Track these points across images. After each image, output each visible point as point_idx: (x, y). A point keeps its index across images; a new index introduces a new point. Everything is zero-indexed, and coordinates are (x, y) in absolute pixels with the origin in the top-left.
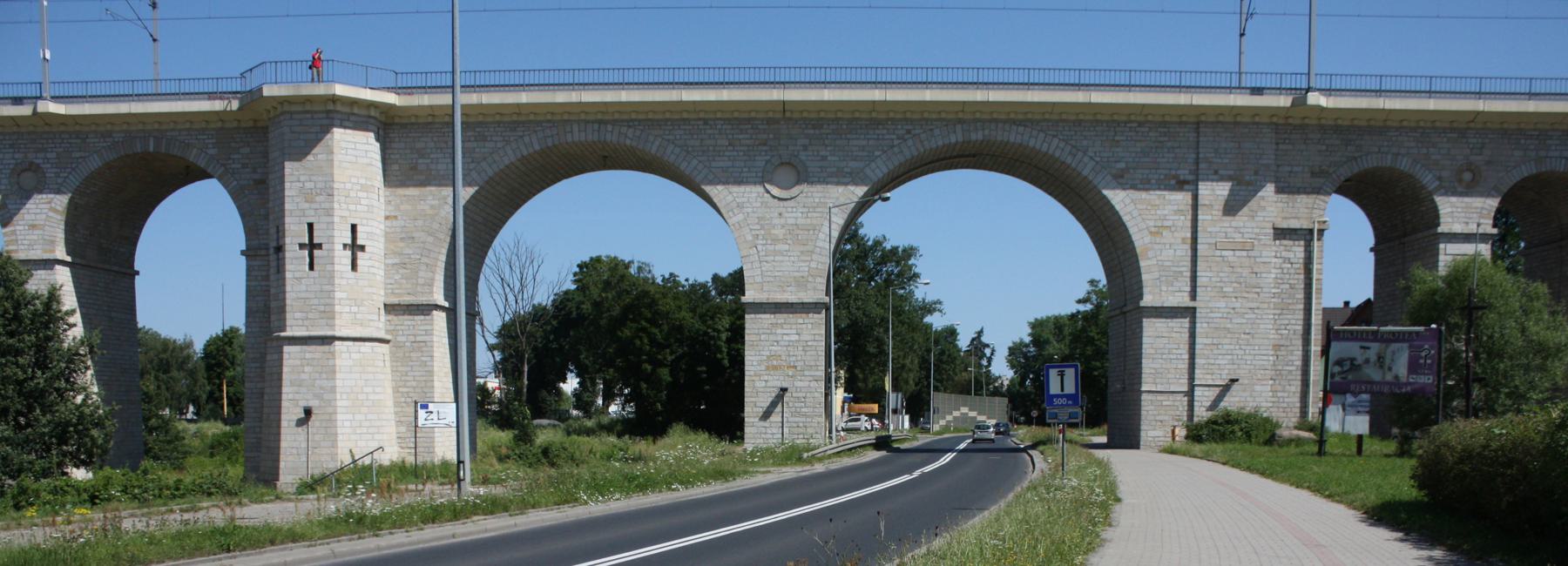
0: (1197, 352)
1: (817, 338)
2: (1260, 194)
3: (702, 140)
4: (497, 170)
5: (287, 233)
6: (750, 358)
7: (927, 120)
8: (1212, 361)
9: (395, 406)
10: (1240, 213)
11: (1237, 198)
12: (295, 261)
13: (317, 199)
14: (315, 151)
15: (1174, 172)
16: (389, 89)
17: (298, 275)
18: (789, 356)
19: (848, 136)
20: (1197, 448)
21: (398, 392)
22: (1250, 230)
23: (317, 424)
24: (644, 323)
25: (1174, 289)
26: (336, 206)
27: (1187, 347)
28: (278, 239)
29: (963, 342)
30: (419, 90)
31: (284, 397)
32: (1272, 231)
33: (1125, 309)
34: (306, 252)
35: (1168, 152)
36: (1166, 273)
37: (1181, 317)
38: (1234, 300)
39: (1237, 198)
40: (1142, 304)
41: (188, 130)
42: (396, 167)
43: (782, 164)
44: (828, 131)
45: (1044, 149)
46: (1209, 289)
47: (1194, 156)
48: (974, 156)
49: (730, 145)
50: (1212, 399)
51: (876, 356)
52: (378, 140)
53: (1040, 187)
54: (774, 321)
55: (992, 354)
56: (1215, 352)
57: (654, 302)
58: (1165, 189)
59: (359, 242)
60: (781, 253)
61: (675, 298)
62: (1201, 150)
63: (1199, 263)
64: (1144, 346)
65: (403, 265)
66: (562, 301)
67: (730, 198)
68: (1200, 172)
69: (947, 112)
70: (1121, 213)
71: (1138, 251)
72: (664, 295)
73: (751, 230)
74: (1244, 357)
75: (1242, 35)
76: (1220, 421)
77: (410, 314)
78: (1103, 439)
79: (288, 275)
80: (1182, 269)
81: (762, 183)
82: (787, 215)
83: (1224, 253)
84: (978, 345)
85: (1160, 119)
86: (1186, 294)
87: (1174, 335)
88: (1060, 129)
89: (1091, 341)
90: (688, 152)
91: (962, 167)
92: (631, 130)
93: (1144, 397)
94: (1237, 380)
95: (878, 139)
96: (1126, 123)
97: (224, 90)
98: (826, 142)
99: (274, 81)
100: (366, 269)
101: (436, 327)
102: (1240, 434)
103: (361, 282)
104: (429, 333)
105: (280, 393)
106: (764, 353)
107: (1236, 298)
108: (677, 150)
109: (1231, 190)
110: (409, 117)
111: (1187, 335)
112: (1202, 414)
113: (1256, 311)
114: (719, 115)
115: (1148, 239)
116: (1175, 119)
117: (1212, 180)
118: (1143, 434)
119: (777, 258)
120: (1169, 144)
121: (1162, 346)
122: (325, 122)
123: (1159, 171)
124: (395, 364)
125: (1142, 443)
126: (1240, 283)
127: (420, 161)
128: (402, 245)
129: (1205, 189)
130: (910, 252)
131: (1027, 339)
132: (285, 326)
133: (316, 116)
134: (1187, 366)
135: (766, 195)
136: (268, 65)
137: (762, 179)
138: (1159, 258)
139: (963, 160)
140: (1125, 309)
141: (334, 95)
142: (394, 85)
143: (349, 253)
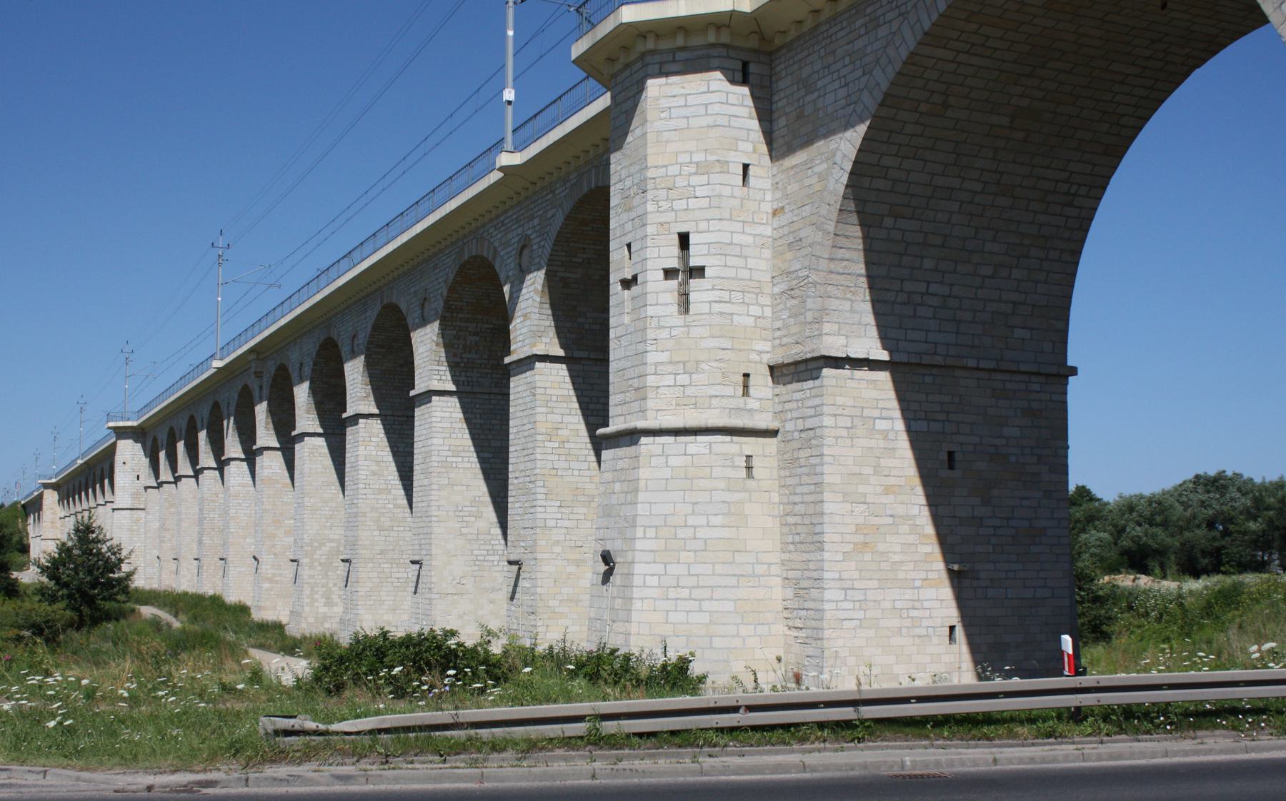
26: (650, 207)
77: (798, 381)
100: (706, 308)
124: (783, 473)
128: (789, 256)
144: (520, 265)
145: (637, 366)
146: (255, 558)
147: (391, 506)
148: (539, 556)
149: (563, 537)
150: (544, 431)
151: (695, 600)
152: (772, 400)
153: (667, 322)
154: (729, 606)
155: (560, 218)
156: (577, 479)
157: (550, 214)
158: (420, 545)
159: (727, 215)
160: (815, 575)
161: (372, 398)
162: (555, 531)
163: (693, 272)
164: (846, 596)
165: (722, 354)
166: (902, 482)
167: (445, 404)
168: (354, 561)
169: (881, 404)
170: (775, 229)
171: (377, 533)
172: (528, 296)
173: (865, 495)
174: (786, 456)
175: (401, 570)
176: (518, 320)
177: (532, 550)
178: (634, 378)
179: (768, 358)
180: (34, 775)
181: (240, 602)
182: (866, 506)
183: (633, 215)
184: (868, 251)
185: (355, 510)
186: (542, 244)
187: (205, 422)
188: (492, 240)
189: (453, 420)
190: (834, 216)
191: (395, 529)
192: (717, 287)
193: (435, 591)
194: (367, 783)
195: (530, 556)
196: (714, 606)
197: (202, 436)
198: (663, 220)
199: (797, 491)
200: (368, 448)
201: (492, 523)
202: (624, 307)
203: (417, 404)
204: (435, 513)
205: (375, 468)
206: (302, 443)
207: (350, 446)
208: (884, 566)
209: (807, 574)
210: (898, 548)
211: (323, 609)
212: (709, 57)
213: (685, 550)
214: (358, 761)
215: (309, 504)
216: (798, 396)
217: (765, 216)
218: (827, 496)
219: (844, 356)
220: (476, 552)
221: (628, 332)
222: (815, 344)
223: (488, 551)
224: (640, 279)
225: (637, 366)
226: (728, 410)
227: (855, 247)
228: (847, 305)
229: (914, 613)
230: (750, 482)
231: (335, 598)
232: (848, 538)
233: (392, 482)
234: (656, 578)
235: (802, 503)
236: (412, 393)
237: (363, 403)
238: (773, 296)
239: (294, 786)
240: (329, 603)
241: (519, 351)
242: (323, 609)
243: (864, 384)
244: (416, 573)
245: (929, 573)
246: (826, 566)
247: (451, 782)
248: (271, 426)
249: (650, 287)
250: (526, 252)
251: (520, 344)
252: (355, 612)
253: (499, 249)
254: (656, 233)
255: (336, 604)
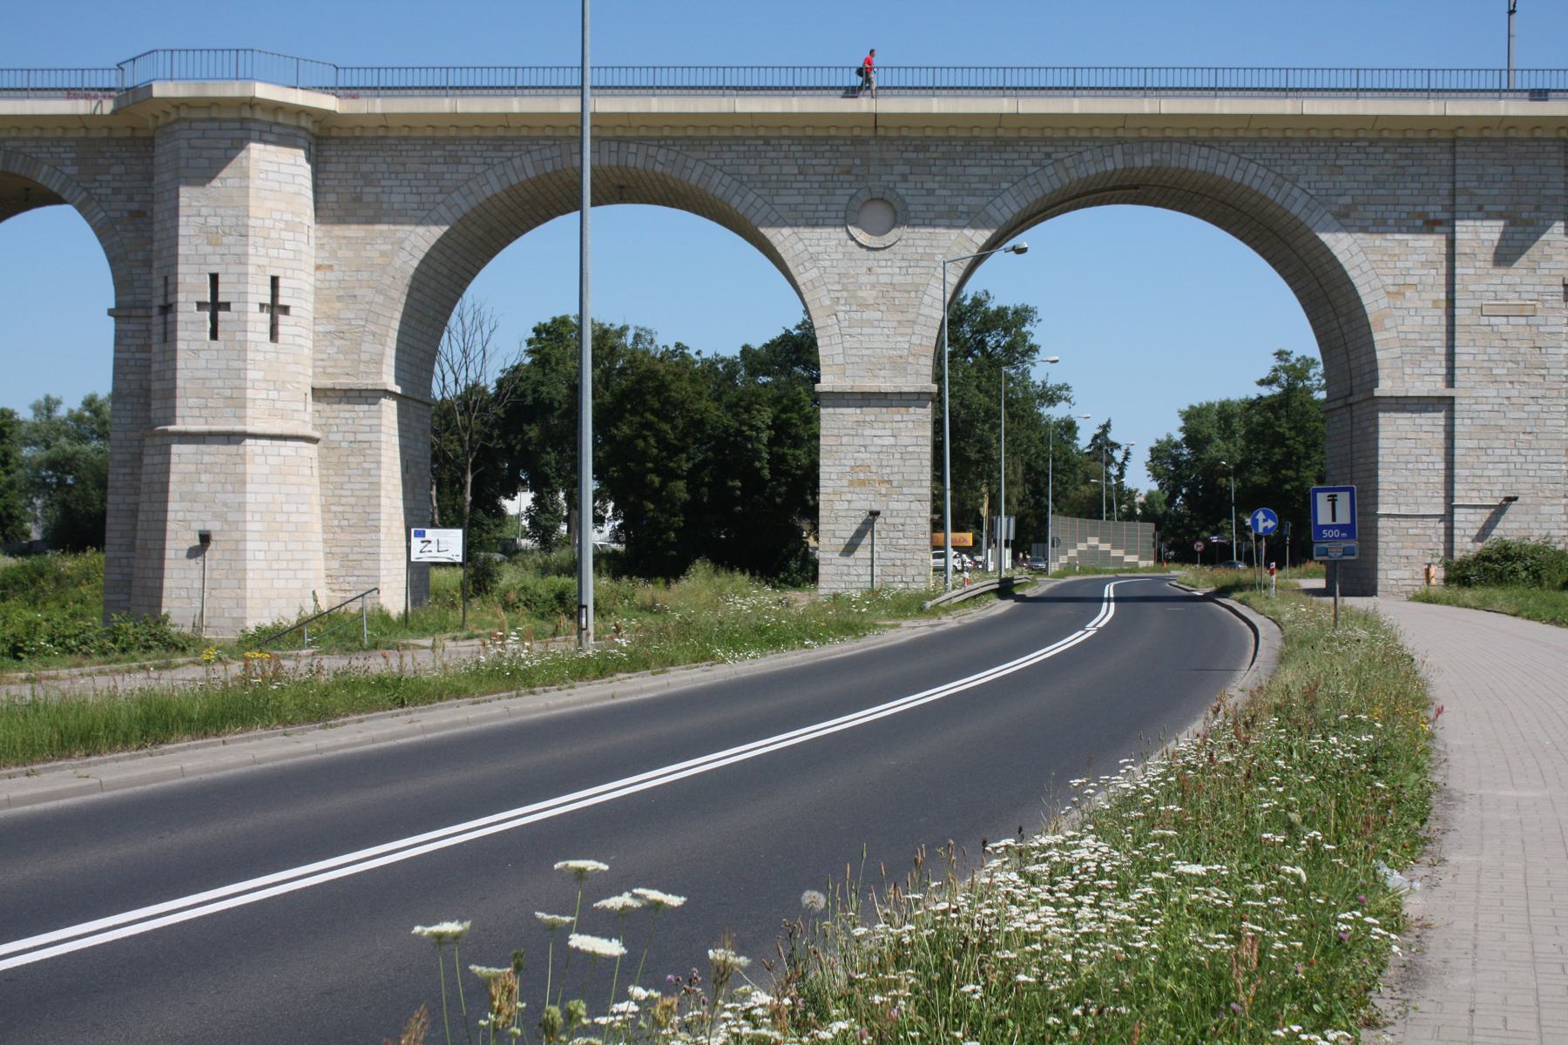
0: (1457, 459)
1: (921, 442)
2: (1544, 237)
3: (761, 166)
4: (474, 204)
5: (180, 288)
6: (827, 469)
7: (1073, 139)
8: (1479, 472)
9: (325, 532)
10: (1516, 265)
11: (1511, 243)
12: (190, 323)
13: (225, 240)
14: (223, 174)
15: (1419, 209)
16: (324, 89)
17: (194, 346)
18: (881, 466)
19: (966, 162)
20: (1468, 594)
21: (329, 511)
22: (1530, 288)
23: (218, 555)
24: (648, 415)
25: (1422, 371)
26: (251, 250)
27: (1442, 452)
28: (166, 295)
29: (1084, 440)
30: (369, 92)
31: (170, 516)
32: (1562, 289)
33: (1351, 400)
34: (207, 314)
35: (1412, 181)
36: (1412, 350)
37: (1434, 411)
38: (1508, 385)
39: (1511, 243)
40: (1377, 393)
41: (37, 139)
42: (332, 197)
43: (872, 199)
44: (935, 155)
45: (1237, 178)
46: (1472, 371)
47: (1449, 186)
48: (1136, 187)
49: (800, 173)
50: (1480, 525)
51: (977, 463)
52: (308, 160)
53: (1228, 228)
54: (861, 418)
55: (1126, 458)
56: (1484, 459)
57: (662, 388)
58: (1408, 232)
59: (282, 301)
60: (870, 323)
61: (693, 381)
62: (1458, 177)
63: (1457, 335)
64: (1381, 452)
65: (340, 334)
66: (512, 378)
67: (800, 246)
68: (1458, 208)
69: (1101, 129)
70: (1346, 267)
71: (1371, 319)
72: (678, 376)
73: (829, 291)
74: (1525, 466)
75: (1511, 12)
76: (1494, 557)
77: (348, 403)
78: (1320, 583)
79: (181, 345)
80: (1434, 343)
81: (844, 223)
82: (879, 271)
83: (1493, 320)
84: (1103, 445)
85: (1399, 136)
86: (1440, 379)
87: (1423, 435)
88: (1260, 150)
89: (1280, 440)
90: (742, 183)
91: (1117, 202)
92: (663, 151)
93: (1382, 523)
94: (1516, 499)
95: (1006, 166)
96: (1351, 141)
97: (93, 85)
98: (934, 169)
99: (168, 76)
100: (290, 340)
101: (384, 422)
102: (1524, 574)
103: (282, 357)
104: (375, 429)
105: (166, 511)
106: (846, 462)
107: (1511, 382)
108: (726, 181)
109: (1503, 233)
110: (352, 129)
111: (1442, 436)
112: (1466, 546)
113: (1541, 401)
114: (785, 132)
115: (1383, 303)
116: (1421, 135)
117: (1475, 219)
118: (1381, 575)
119: (866, 330)
120: (1412, 170)
121: (1406, 451)
122: (238, 134)
123: (1398, 208)
124: (325, 472)
125: (1379, 588)
126: (1517, 363)
127: (367, 190)
128: (338, 305)
129: (1465, 231)
130: (1023, 315)
131: (1179, 436)
132: (174, 416)
133: (225, 125)
134: (1442, 479)
135: (850, 242)
136: (161, 53)
137: (845, 220)
138: (1400, 328)
139: (1118, 192)
140: (1351, 400)
141: (253, 98)
142: (333, 84)
143: (267, 316)
198: (260, 263)
212: (296, 136)
241: (489, 382)
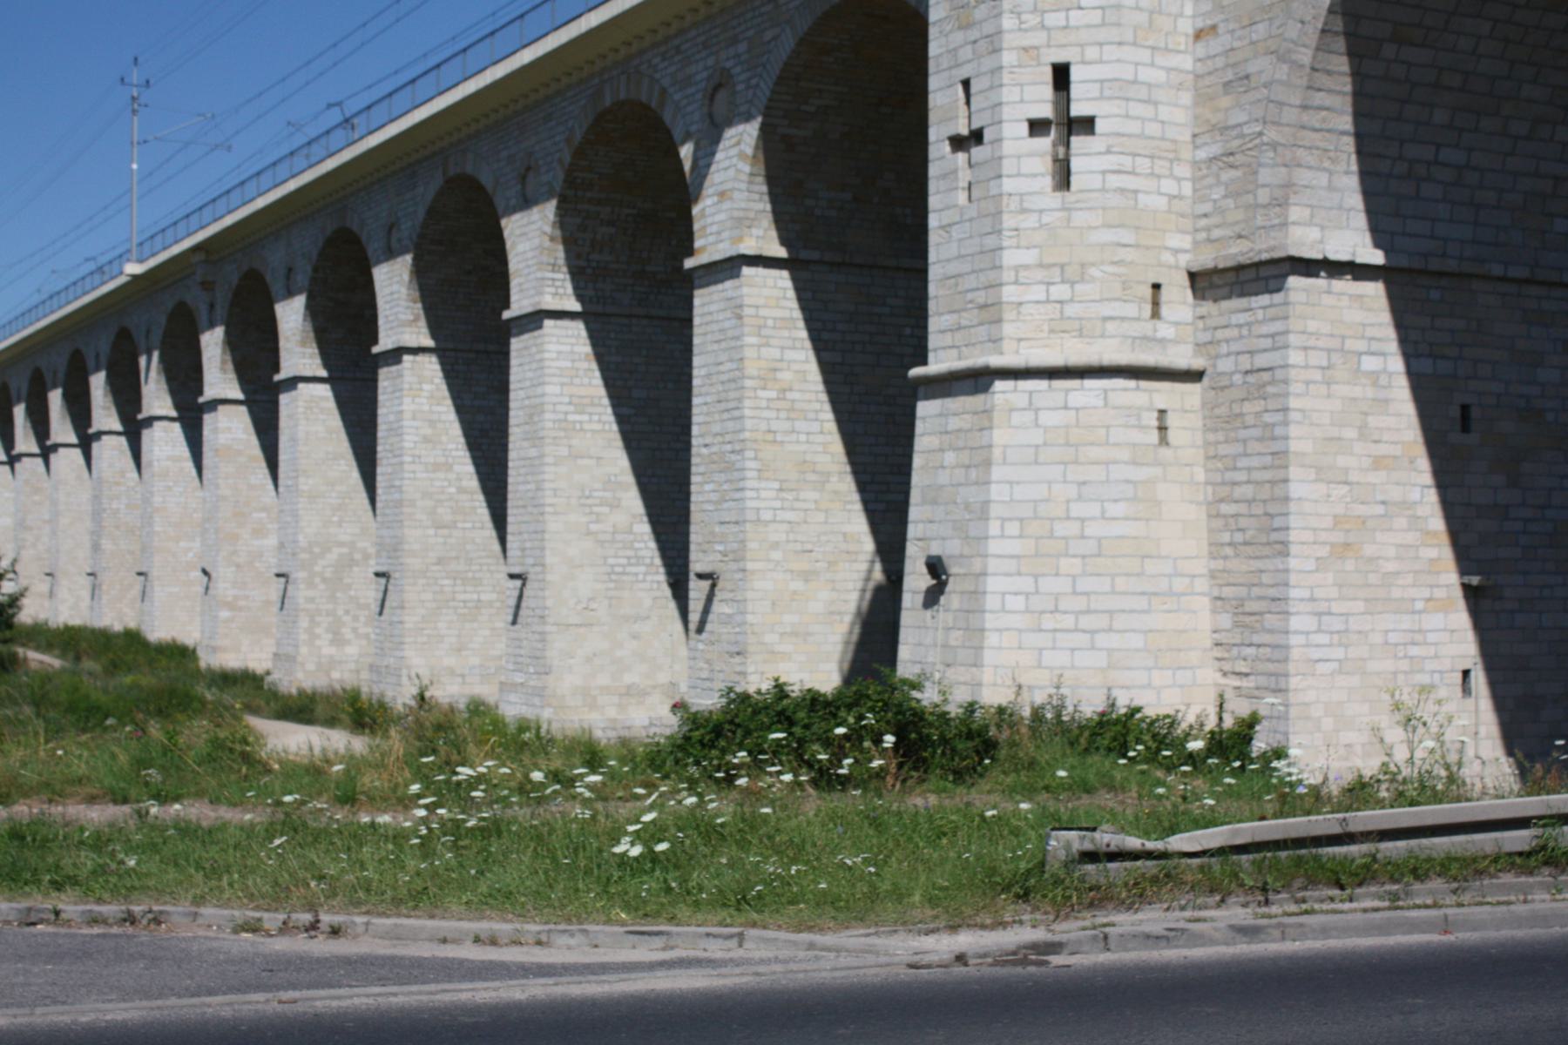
26: (1008, 22)
77: (1242, 295)
100: (1096, 182)
124: (1211, 437)
128: (1225, 102)
144: (711, 116)
145: (981, 270)
146: (205, 572)
147: (453, 490)
148: (750, 566)
149: (784, 537)
150: (755, 373)
151: (1084, 631)
152: (1192, 324)
153: (1032, 203)
154: (1136, 641)
155: (788, 43)
156: (804, 447)
157: (768, 35)
158: (523, 550)
159: (1129, 37)
160: (1272, 592)
161: (423, 323)
162: (772, 527)
163: (1075, 127)
164: (1320, 625)
165: (1123, 254)
166: (1397, 450)
167: (563, 332)
168: (531, 577)
169: (1370, 332)
170: (1200, 60)
171: (431, 532)
172: (727, 163)
173: (1346, 470)
174: (1217, 411)
175: (469, 589)
176: (709, 202)
177: (739, 556)
178: (978, 289)
179: (1185, 260)
180: (720, 941)
181: (174, 641)
182: (1346, 488)
183: (974, 34)
184: (1358, 95)
185: (397, 496)
186: (754, 82)
187: (103, 359)
188: (657, 76)
189: (577, 357)
190: (1312, 37)
191: (460, 525)
192: (1114, 149)
193: (550, 620)
194: (1283, 939)
195: (733, 566)
196: (1113, 640)
197: (98, 383)
198: (1026, 43)
199: (1239, 465)
200: (417, 400)
201: (634, 516)
202: (957, 179)
203: (514, 331)
204: (548, 501)
205: (428, 431)
206: (293, 393)
207: (385, 397)
208: (1372, 578)
209: (1256, 591)
210: (1392, 552)
211: (328, 650)
213: (1067, 555)
214: (1223, 901)
215: (305, 488)
216: (1242, 318)
217: (1182, 39)
218: (1294, 472)
219: (1320, 256)
220: (611, 561)
221: (966, 217)
222: (1275, 238)
223: (629, 558)
224: (987, 136)
225: (981, 270)
226: (1130, 341)
227: (1338, 88)
228: (1323, 179)
229: (1414, 651)
230: (1165, 452)
231: (347, 633)
232: (1323, 536)
233: (454, 453)
234: (1021, 598)
235: (1248, 482)
236: (506, 315)
237: (408, 329)
238: (1195, 164)
239: (1177, 947)
240: (338, 640)
242: (328, 650)
243: (1345, 301)
244: (516, 593)
245: (1435, 590)
246: (1293, 579)
247: (1404, 933)
248: (230, 366)
249: (1008, 147)
250: (722, 96)
251: (711, 239)
252: (398, 653)
253: (671, 90)
254: (1016, 63)
255: (348, 642)
